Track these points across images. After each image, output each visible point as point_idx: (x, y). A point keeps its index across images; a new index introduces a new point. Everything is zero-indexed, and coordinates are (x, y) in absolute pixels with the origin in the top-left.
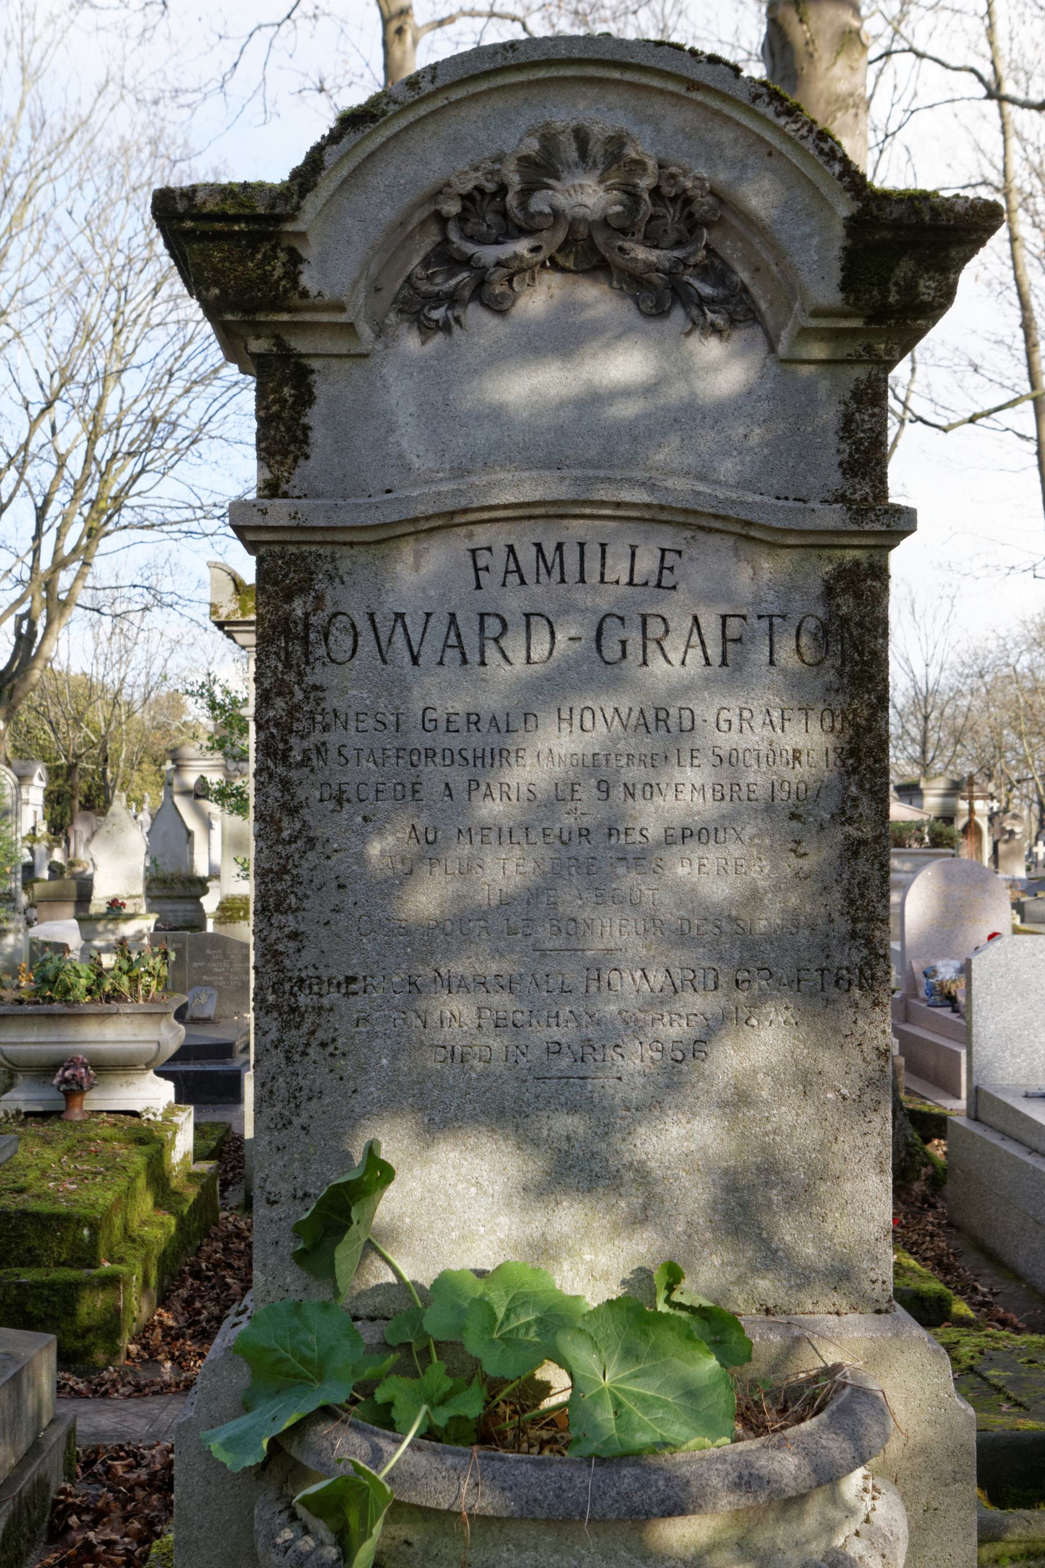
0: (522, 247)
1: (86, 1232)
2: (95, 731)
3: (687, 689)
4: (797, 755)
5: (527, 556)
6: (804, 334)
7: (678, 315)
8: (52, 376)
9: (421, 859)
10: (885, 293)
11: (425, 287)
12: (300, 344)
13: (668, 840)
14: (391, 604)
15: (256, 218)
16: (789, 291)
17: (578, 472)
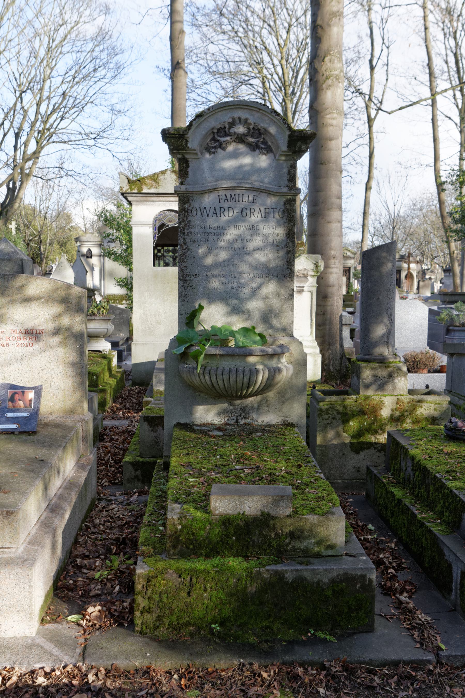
0: (228, 138)
1: (95, 377)
2: (35, 230)
3: (258, 222)
4: (278, 234)
5: (229, 196)
6: (281, 155)
7: (257, 151)
8: (20, 75)
9: (208, 253)
10: (295, 148)
11: (210, 145)
12: (187, 156)
13: (254, 250)
14: (203, 205)
15: (180, 134)
16: (278, 147)
17: (238, 181)
